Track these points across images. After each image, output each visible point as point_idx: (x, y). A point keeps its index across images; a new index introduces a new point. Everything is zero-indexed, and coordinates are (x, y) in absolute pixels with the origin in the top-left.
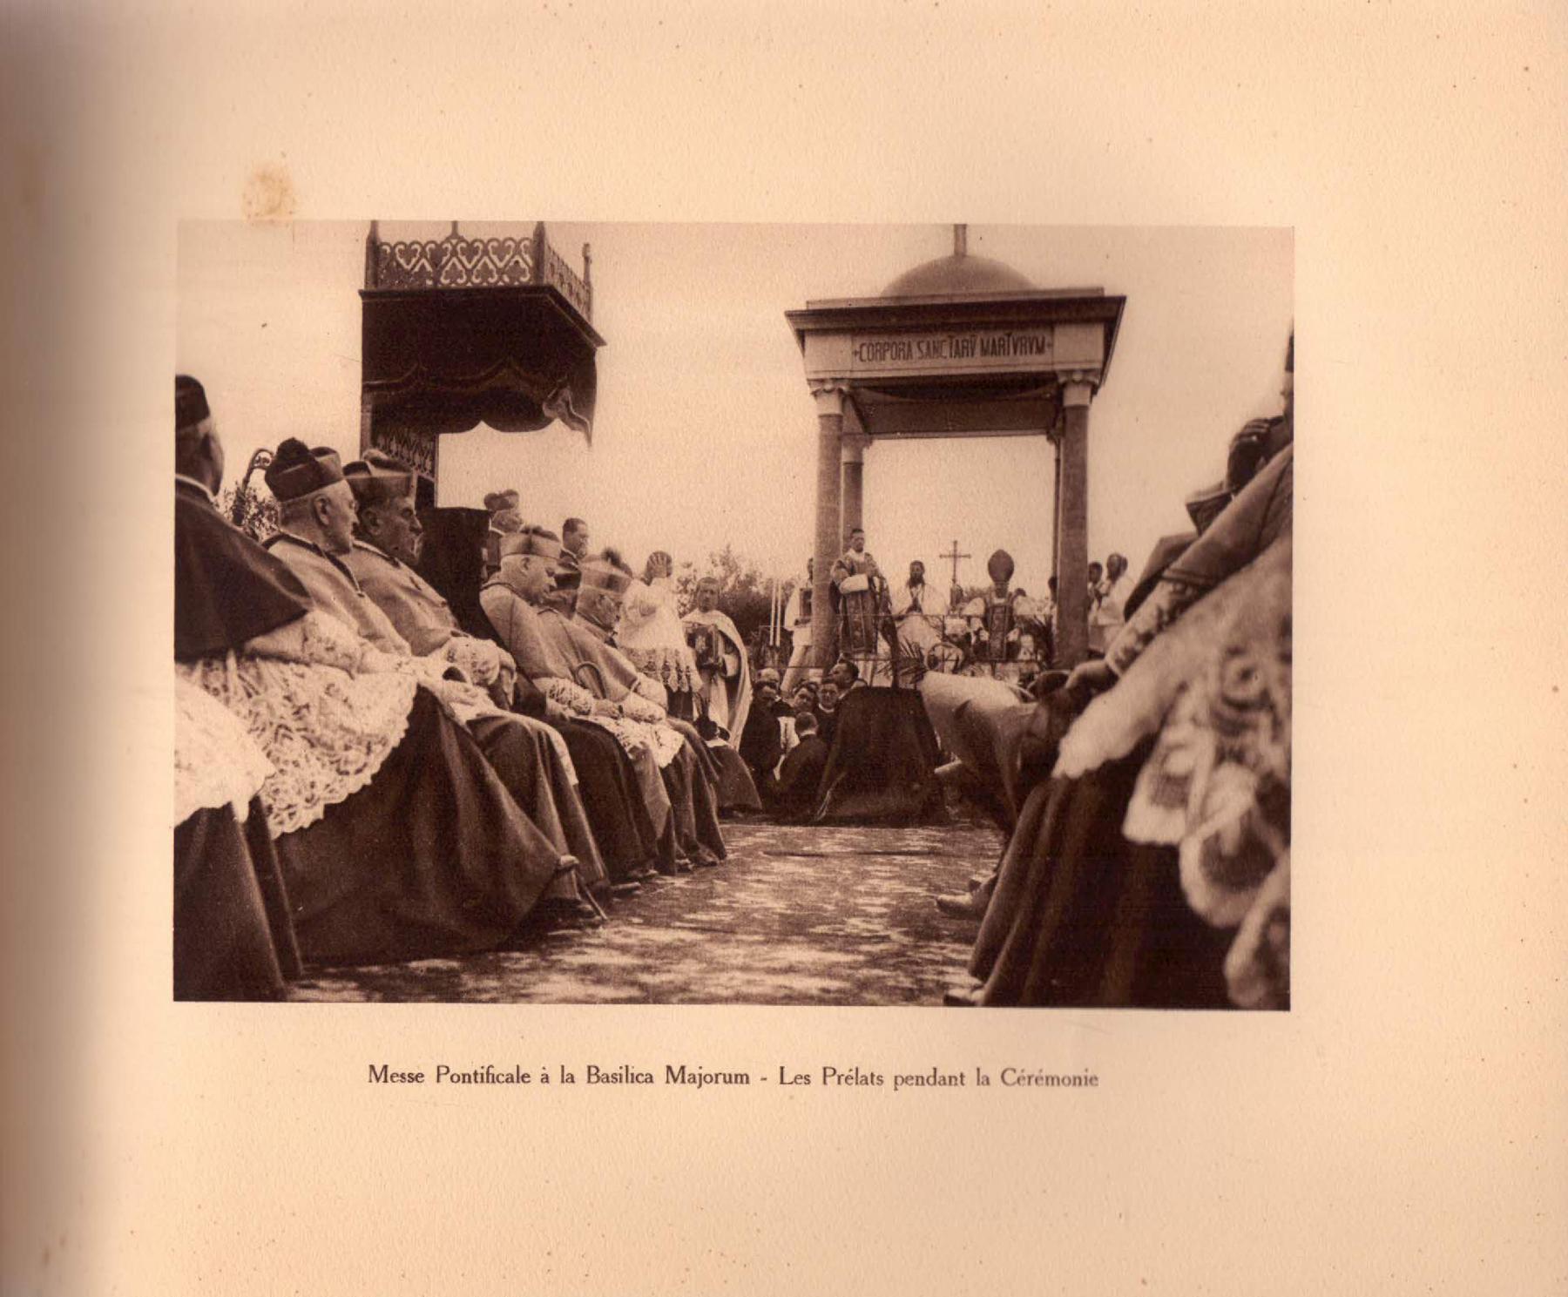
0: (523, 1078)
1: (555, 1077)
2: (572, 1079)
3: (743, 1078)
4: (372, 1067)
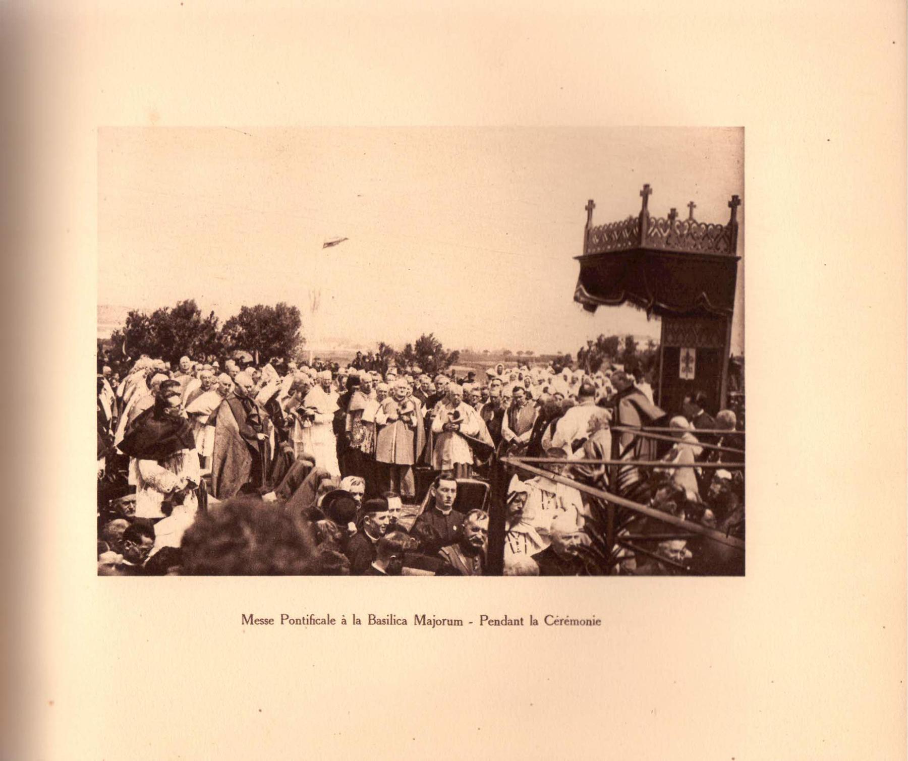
0: (332, 621)
1: (350, 621)
2: (359, 622)
3: (459, 623)
4: (244, 616)
